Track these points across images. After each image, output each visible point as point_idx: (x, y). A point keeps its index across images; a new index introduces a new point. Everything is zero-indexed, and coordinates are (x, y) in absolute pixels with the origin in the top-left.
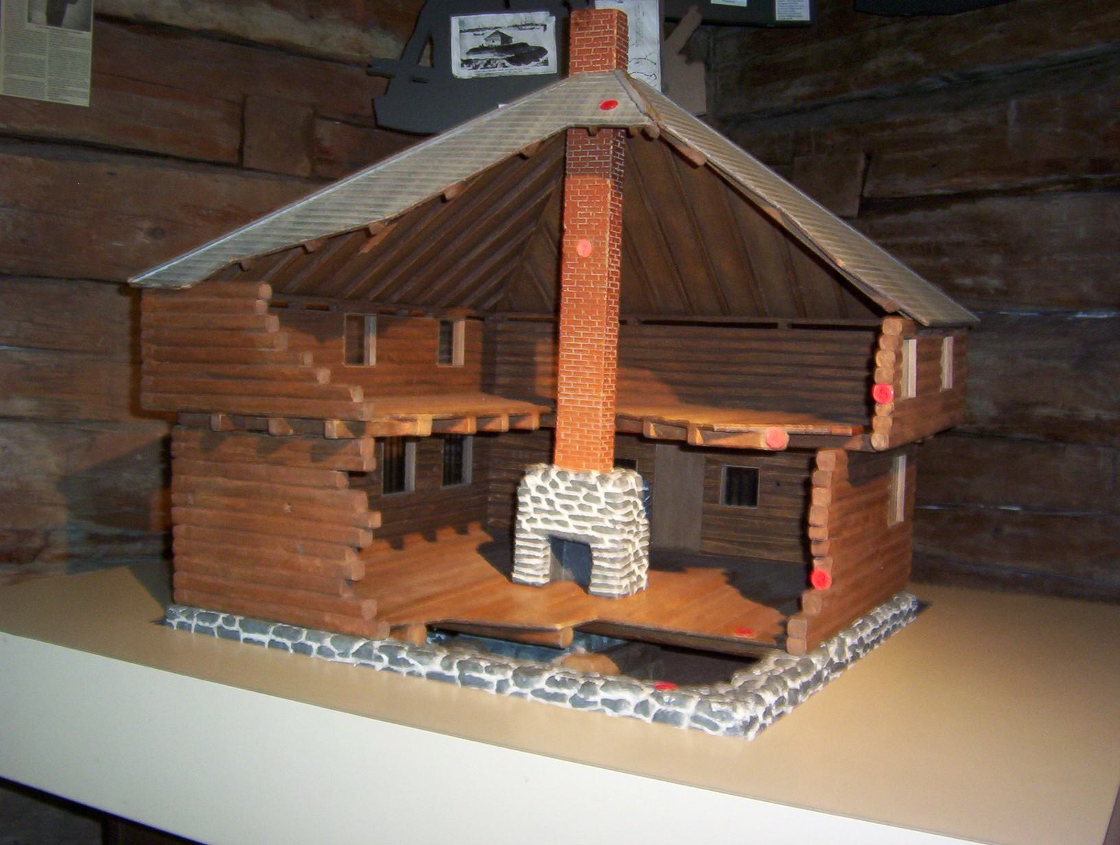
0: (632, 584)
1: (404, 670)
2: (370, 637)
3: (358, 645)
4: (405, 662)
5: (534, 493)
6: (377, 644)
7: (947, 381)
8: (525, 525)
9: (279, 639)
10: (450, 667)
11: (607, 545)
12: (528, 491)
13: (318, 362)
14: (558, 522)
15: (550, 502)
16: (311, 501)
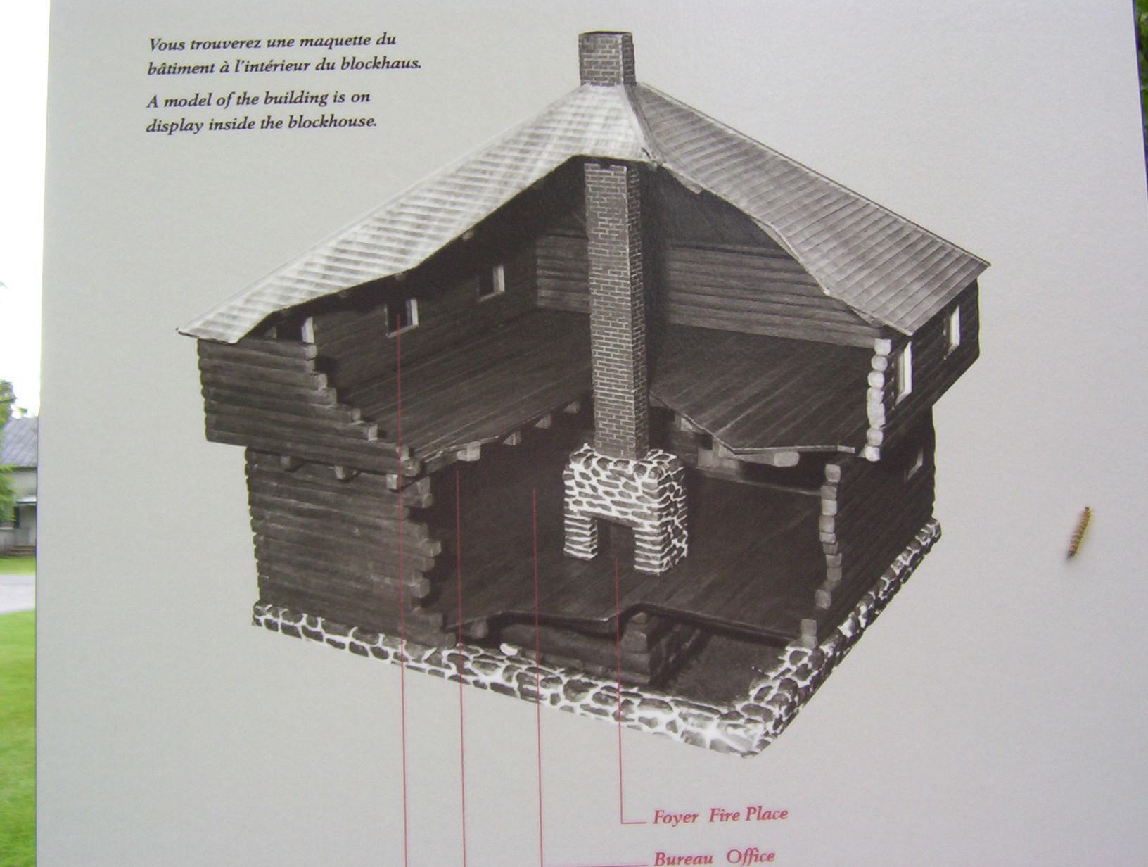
0: (673, 559)
1: (470, 678)
2: (441, 646)
3: (428, 653)
4: (470, 672)
5: (578, 478)
6: (445, 653)
8: (572, 507)
9: (358, 642)
10: (509, 679)
12: (572, 477)
13: (368, 420)
14: (601, 506)
15: (594, 488)
16: (377, 528)
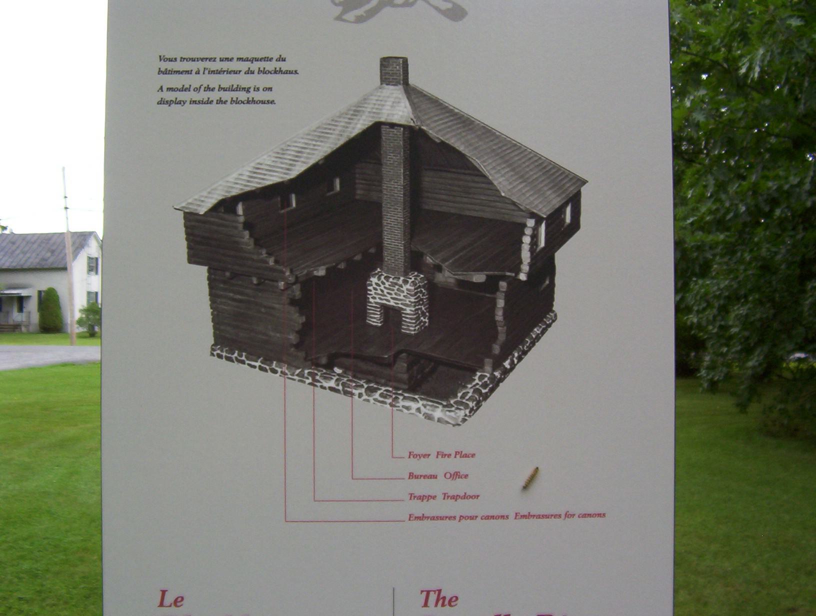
3: (298, 371)
4: (319, 381)
6: (306, 371)
7: (542, 244)
10: (338, 385)
11: (408, 312)
13: (270, 254)
15: (382, 291)
